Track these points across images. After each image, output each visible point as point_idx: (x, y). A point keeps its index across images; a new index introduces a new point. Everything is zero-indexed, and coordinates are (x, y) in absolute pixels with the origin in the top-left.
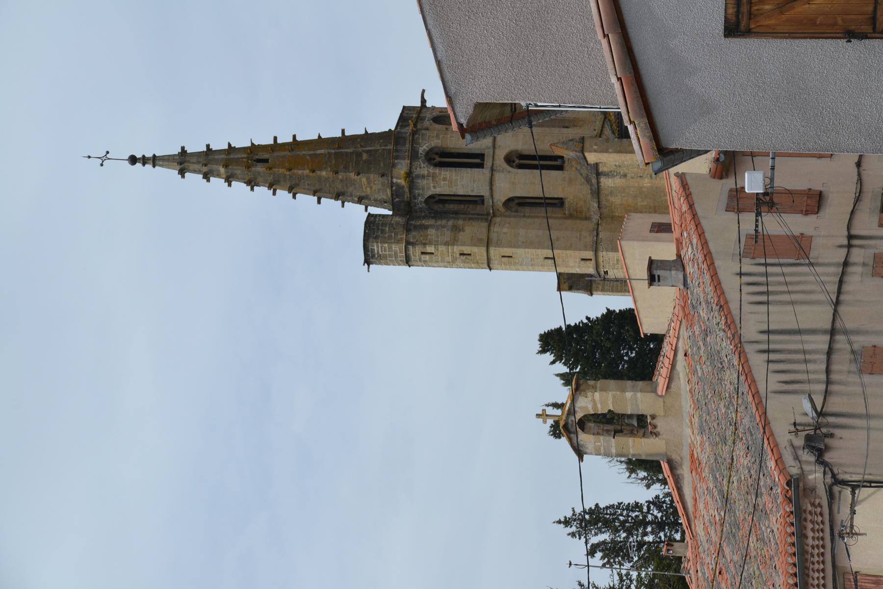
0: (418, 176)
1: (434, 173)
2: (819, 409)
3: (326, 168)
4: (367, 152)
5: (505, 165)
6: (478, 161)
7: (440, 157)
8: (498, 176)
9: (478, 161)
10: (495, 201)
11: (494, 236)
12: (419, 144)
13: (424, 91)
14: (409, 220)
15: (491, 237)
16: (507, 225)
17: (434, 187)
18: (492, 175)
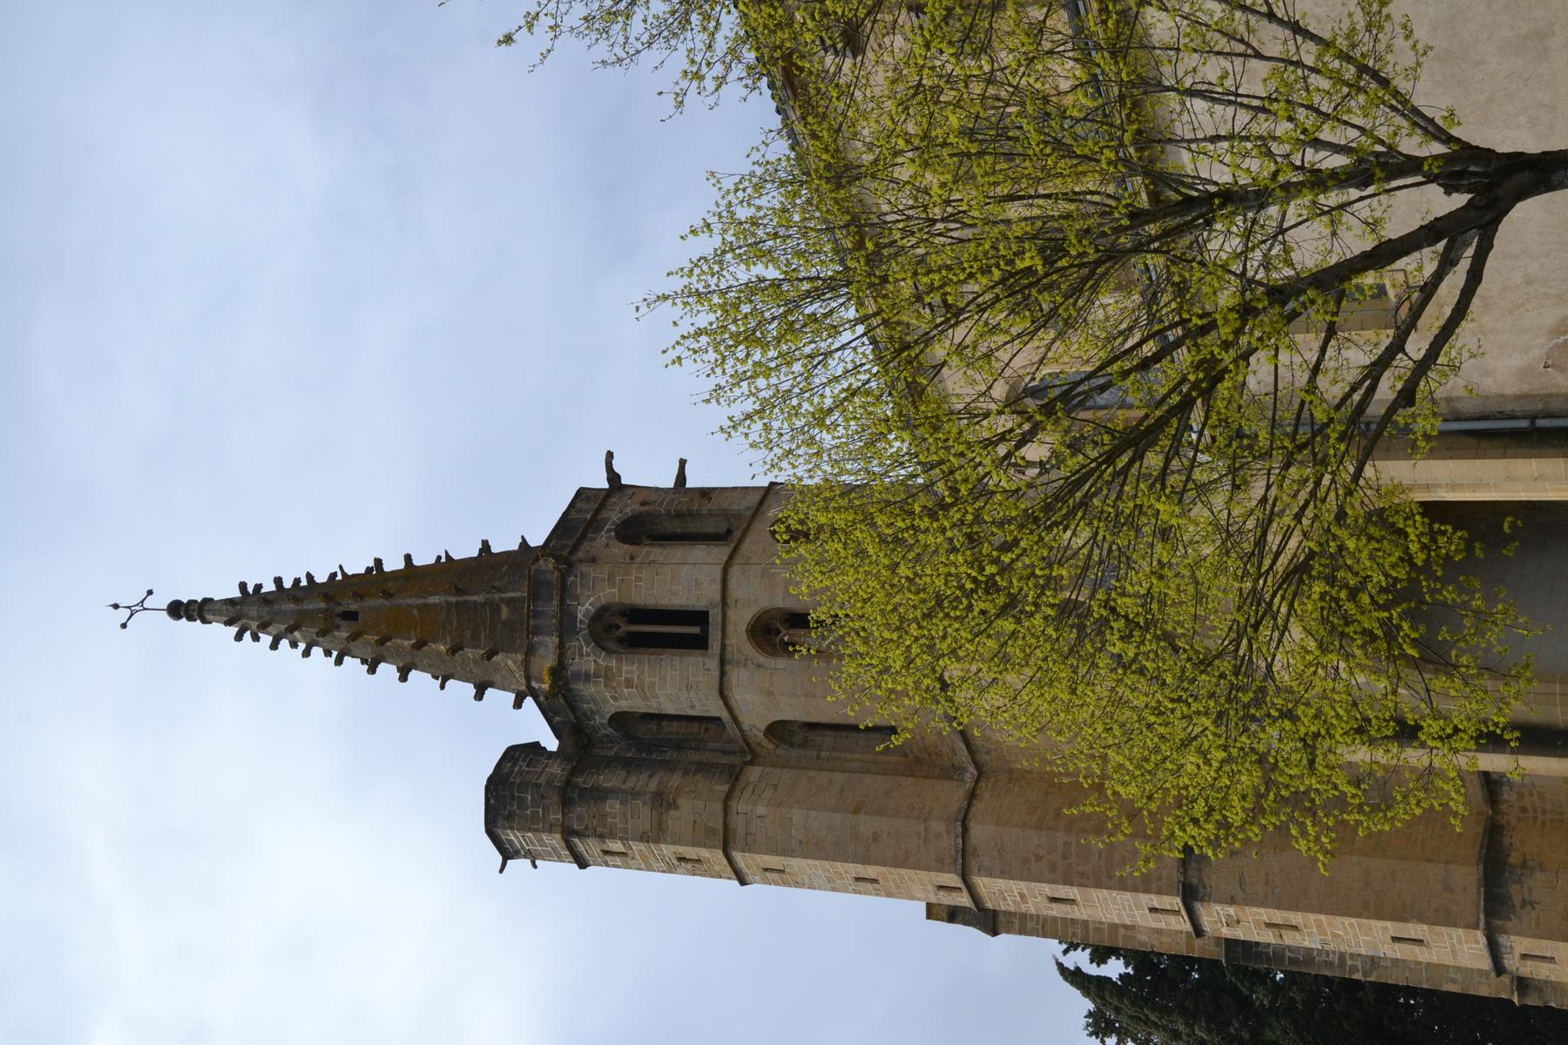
0: (578, 676)
1: (608, 669)
2: (1285, 226)
3: (444, 638)
4: (510, 602)
5: (749, 649)
6: (696, 630)
7: (631, 622)
8: (736, 676)
9: (696, 630)
10: (746, 727)
11: (738, 823)
12: (577, 598)
13: (610, 455)
14: (573, 772)
15: (732, 826)
16: (769, 794)
17: (615, 699)
18: (723, 674)
